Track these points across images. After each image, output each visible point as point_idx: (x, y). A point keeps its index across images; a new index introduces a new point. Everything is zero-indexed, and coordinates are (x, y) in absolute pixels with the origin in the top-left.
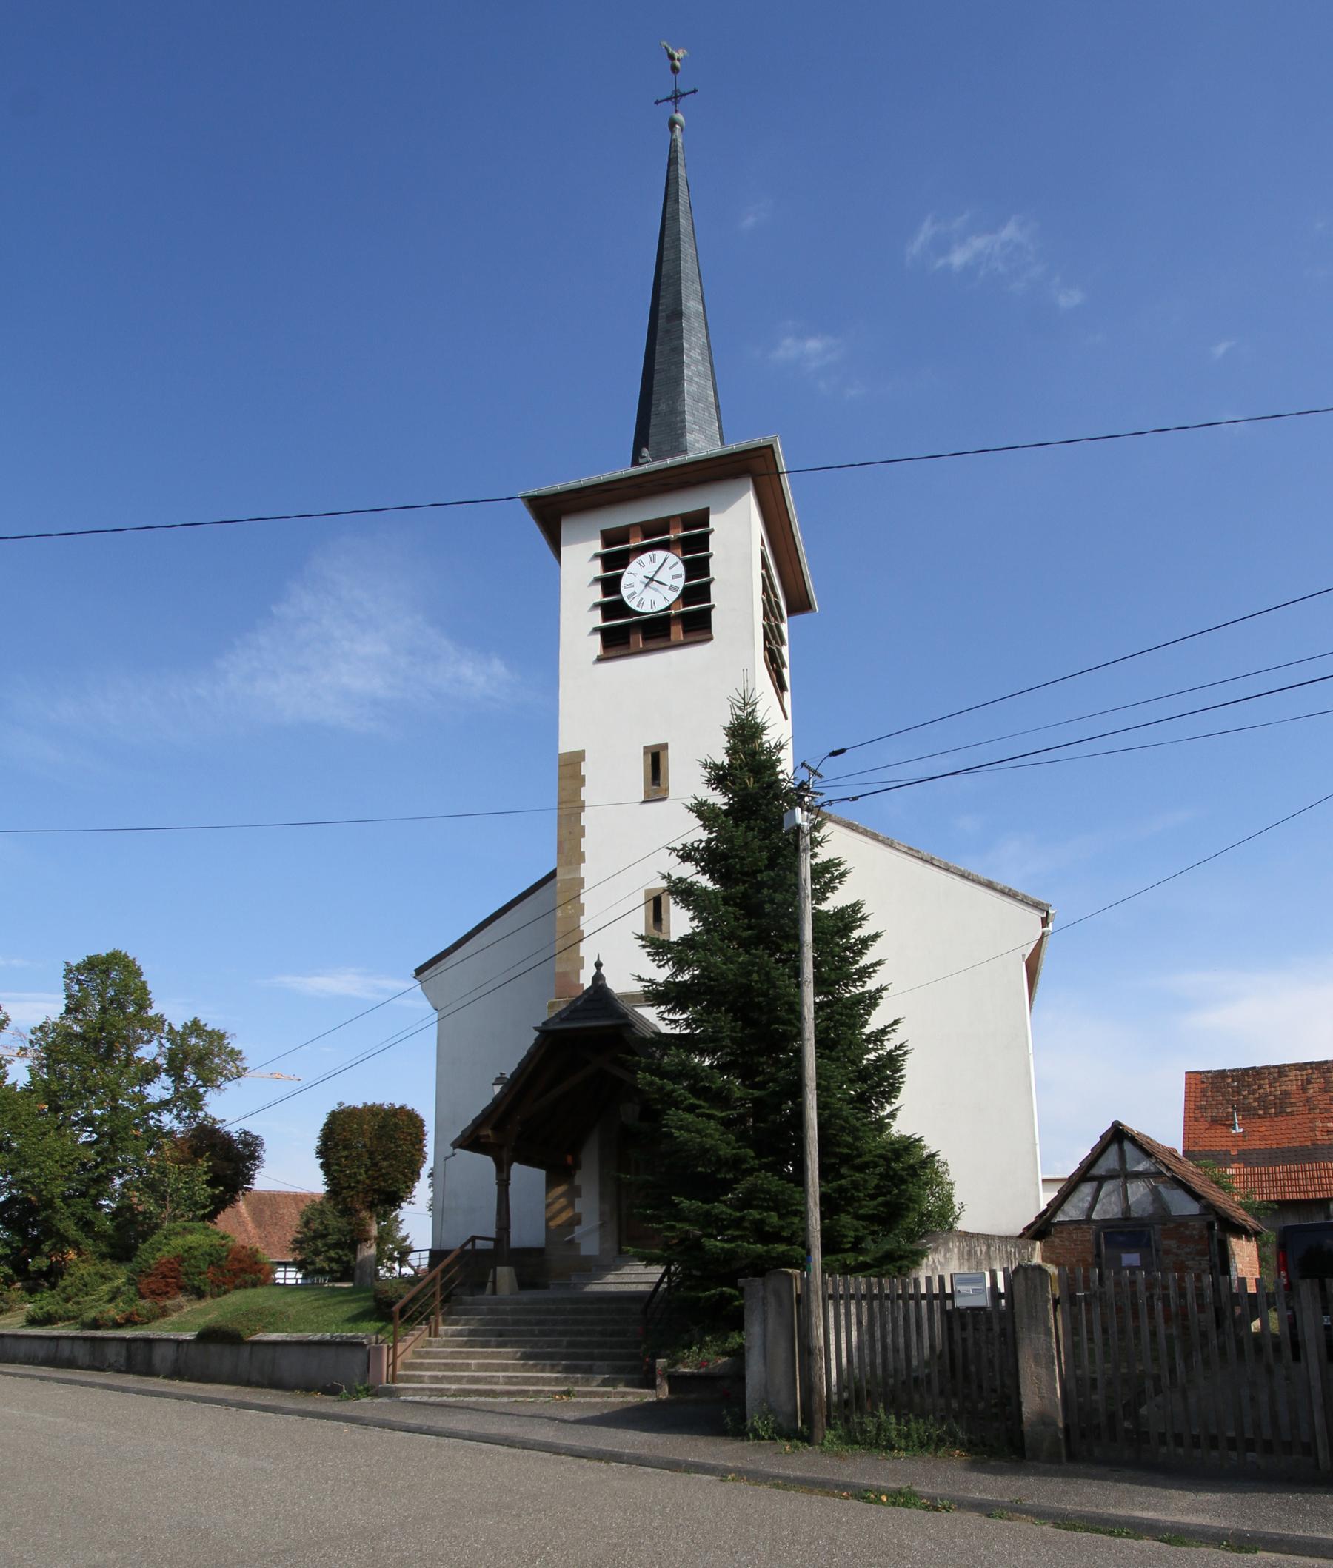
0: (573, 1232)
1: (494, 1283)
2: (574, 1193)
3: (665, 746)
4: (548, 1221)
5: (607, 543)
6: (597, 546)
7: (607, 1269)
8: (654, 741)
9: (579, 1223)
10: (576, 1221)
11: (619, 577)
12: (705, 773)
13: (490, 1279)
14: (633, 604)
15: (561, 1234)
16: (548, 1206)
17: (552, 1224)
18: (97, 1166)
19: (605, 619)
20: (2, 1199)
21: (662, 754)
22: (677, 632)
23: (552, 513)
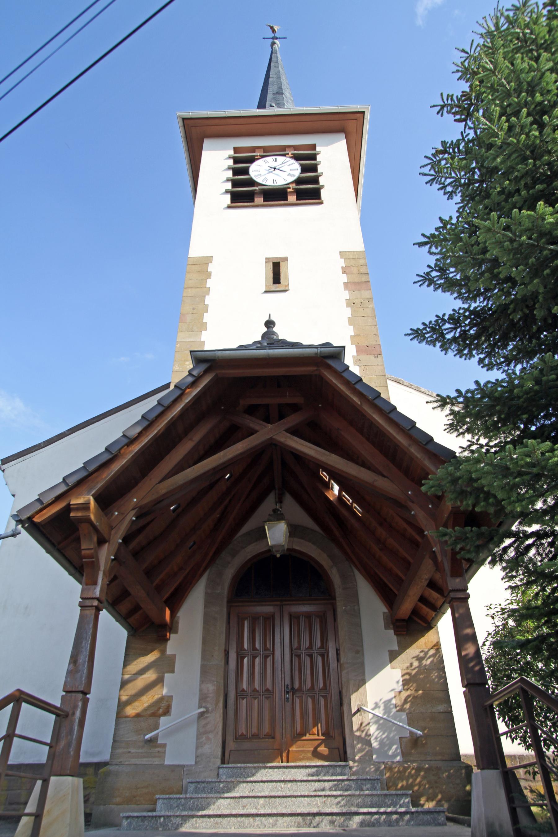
0: (156, 727)
1: (38, 816)
2: (166, 665)
3: (285, 259)
4: (122, 705)
5: (235, 152)
6: (231, 152)
7: (220, 789)
8: (276, 254)
9: (167, 712)
10: (163, 708)
11: (248, 167)
12: (342, 263)
13: (31, 808)
14: (259, 180)
15: (140, 726)
16: (124, 684)
17: (130, 711)
18: (538, 535)
19: (233, 187)
20: (557, 445)
21: (282, 265)
22: (292, 198)
23: (197, 134)
